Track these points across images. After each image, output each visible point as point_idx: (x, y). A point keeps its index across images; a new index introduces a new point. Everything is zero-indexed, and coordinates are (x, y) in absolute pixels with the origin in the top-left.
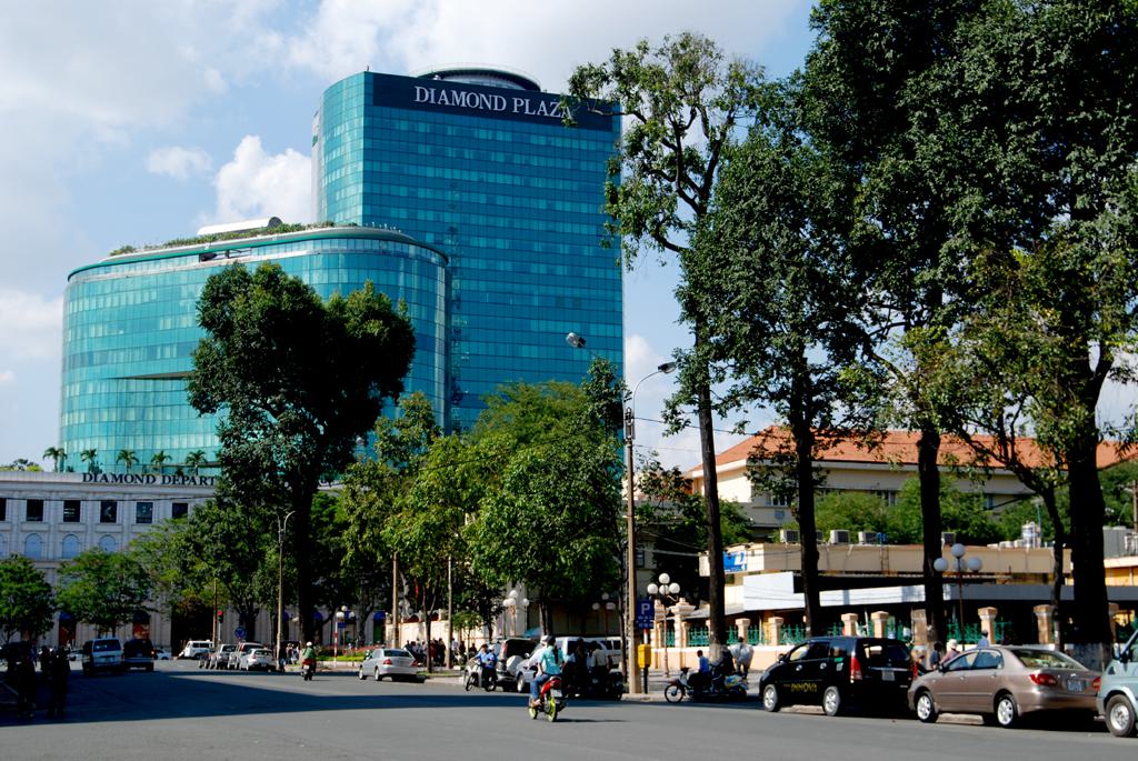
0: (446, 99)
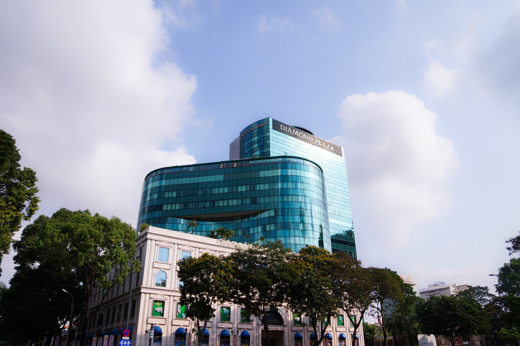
0: (291, 131)
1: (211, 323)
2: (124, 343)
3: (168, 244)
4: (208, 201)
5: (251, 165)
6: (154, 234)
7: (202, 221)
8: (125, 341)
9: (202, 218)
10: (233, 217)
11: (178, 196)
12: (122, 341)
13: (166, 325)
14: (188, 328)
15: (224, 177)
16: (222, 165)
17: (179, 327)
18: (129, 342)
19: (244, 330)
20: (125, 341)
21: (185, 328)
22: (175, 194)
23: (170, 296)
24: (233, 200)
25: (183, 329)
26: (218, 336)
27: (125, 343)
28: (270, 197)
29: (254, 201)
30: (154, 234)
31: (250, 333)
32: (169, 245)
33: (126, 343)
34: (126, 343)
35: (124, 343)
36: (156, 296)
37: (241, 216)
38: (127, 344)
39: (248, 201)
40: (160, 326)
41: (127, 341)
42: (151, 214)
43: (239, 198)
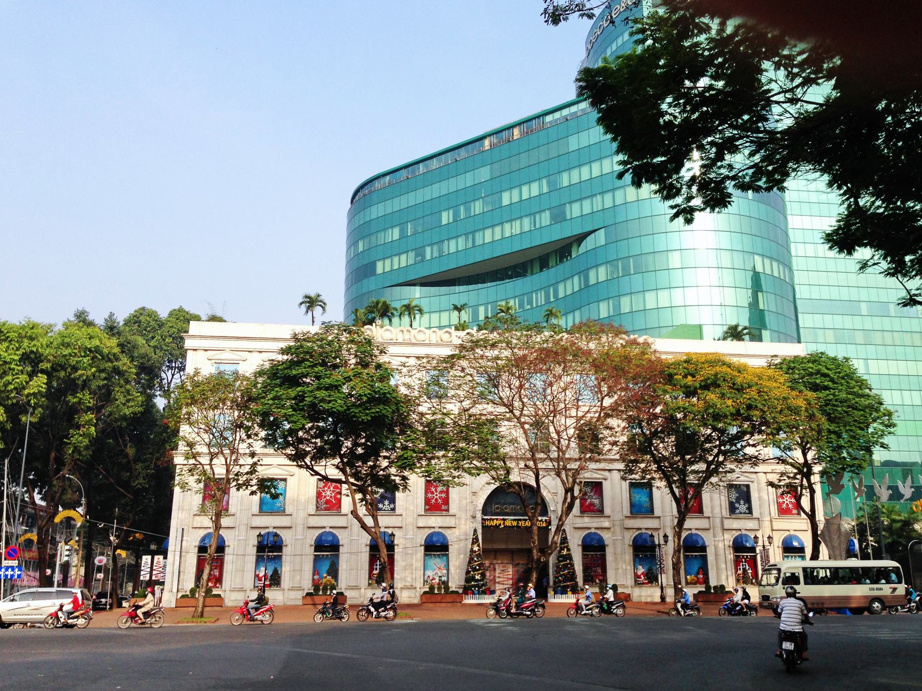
1: (707, 520)
2: (7, 573)
3: (234, 354)
4: (461, 235)
5: (555, 124)
6: (201, 337)
7: (459, 285)
8: (10, 570)
9: (459, 278)
11: (403, 236)
12: (3, 570)
13: (711, 530)
14: (759, 534)
16: (487, 142)
17: (788, 533)
18: (17, 570)
20: (10, 570)
23: (610, 470)
24: (514, 223)
25: (746, 536)
27: (10, 573)
29: (559, 216)
30: (201, 337)
33: (12, 573)
34: (12, 573)
35: (7, 573)
36: (268, 469)
38: (12, 576)
39: (545, 219)
40: (599, 532)
41: (13, 568)
43: (526, 216)
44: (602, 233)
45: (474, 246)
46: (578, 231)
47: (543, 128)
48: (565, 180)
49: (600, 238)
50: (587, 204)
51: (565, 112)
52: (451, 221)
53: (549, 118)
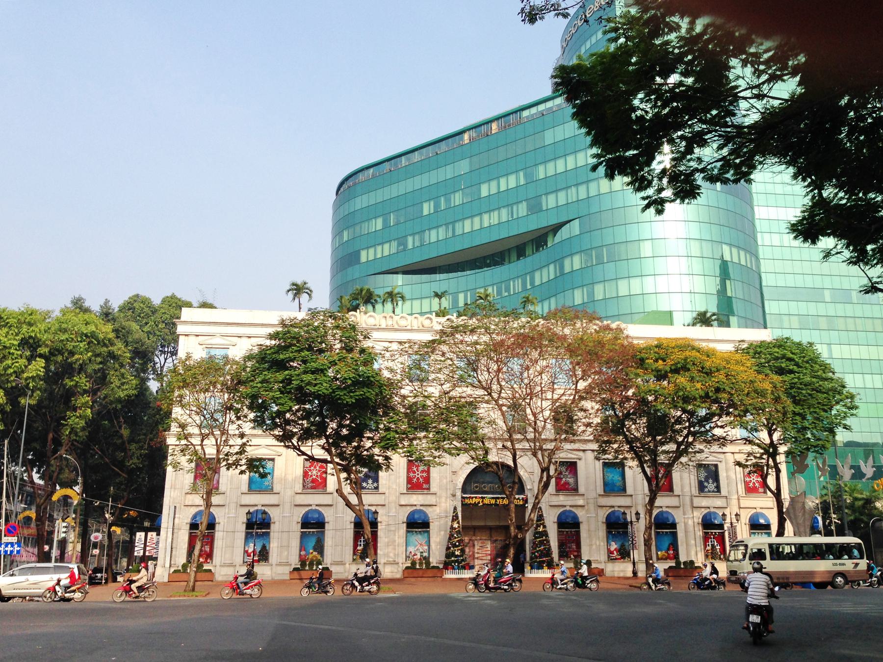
2: (6, 549)
3: (224, 339)
5: (532, 118)
8: (9, 546)
10: (501, 252)
11: (386, 226)
15: (471, 163)
16: (466, 136)
17: (755, 511)
18: (16, 546)
19: (708, 510)
20: (9, 546)
21: (373, 509)
22: (379, 224)
24: (492, 214)
26: (696, 524)
27: (9, 549)
28: (569, 191)
29: (535, 207)
31: (581, 514)
32: (227, 340)
33: (12, 549)
34: (12, 549)
35: (6, 549)
36: (255, 450)
37: (517, 247)
38: (12, 552)
39: (522, 209)
41: (12, 544)
42: (572, 267)
44: (576, 223)
45: (454, 236)
46: (553, 221)
47: (520, 123)
48: (541, 172)
49: (575, 228)
50: (562, 196)
51: (541, 107)
52: (432, 211)
53: (525, 113)
